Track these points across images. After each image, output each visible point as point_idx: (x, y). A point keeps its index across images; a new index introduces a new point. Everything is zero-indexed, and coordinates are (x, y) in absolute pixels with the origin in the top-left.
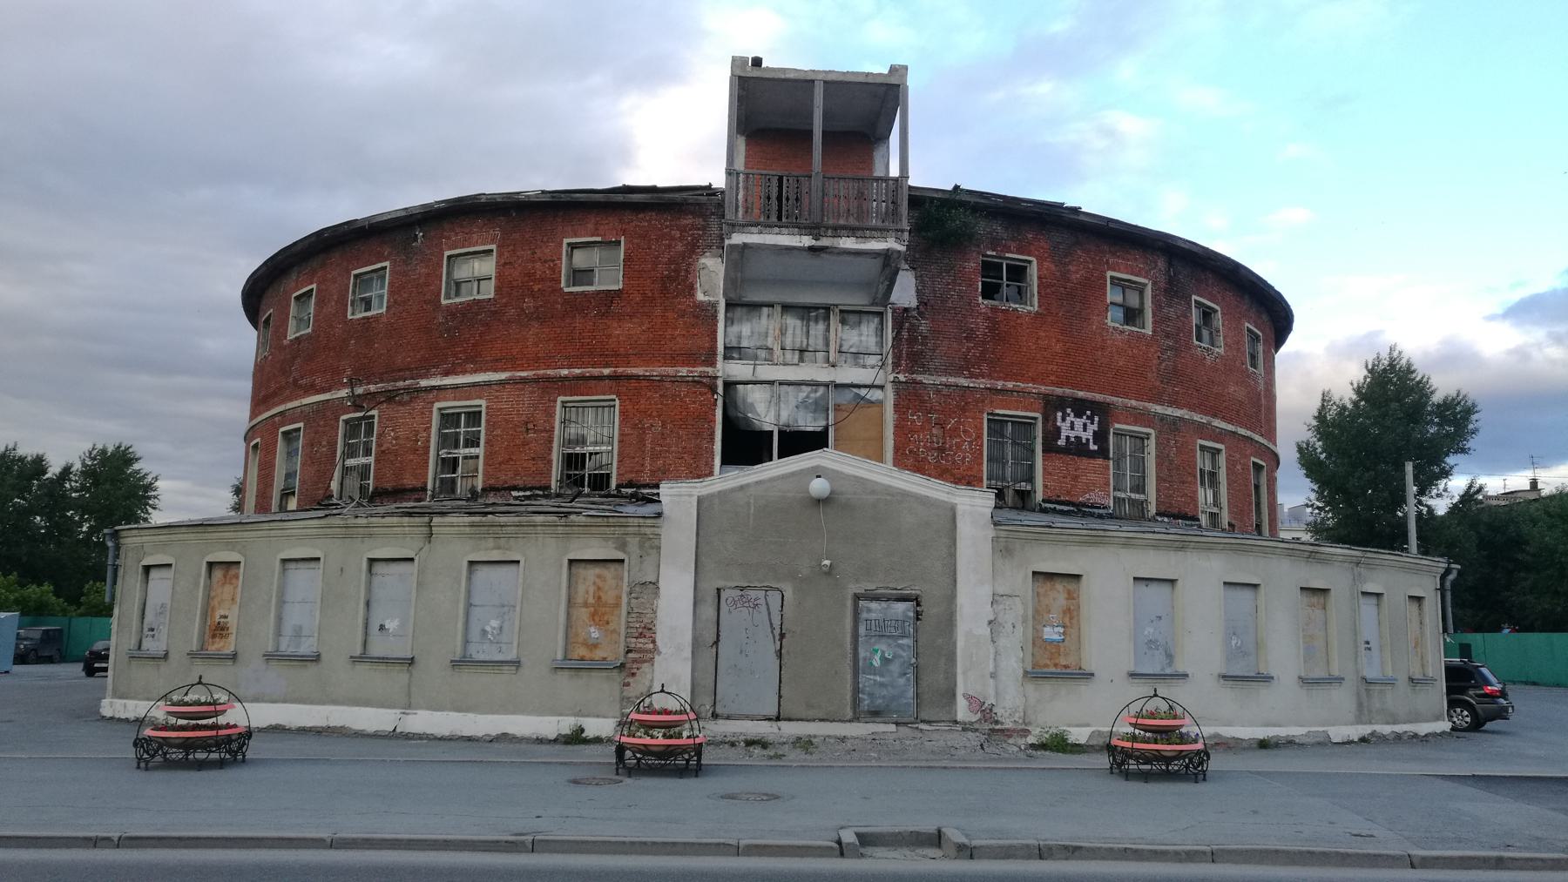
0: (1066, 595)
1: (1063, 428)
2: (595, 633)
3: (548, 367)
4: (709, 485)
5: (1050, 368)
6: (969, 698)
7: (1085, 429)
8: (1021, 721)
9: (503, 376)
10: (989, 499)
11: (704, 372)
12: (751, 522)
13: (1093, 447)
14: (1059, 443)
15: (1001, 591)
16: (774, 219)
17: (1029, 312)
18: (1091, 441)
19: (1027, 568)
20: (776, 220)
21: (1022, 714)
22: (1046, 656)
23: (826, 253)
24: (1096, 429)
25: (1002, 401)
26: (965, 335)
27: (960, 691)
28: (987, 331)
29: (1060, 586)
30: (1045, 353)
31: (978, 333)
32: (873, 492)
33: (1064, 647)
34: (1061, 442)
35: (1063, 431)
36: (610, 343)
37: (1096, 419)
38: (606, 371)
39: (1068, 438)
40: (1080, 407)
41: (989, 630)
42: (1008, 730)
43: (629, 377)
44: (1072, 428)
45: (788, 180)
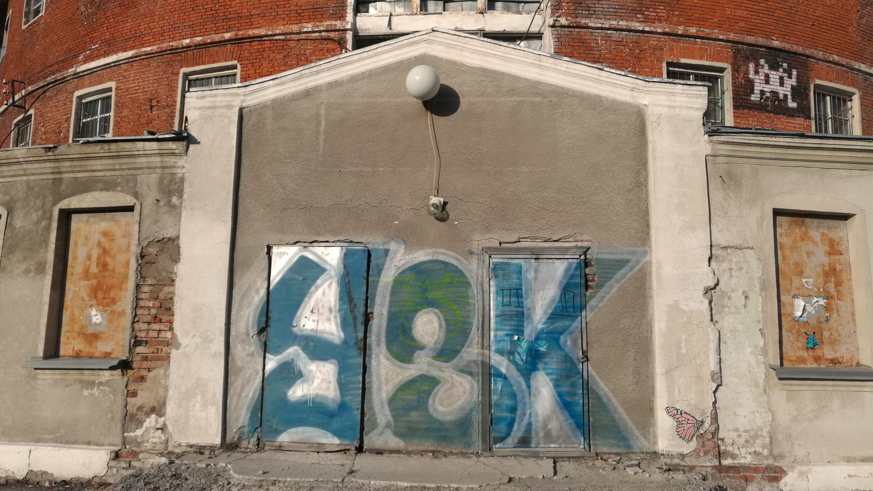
0: (827, 248)
1: (756, 81)
2: (96, 317)
3: (173, 39)
4: (258, 91)
5: (739, 13)
6: (674, 412)
7: (782, 84)
8: (766, 452)
9: (130, 54)
10: (698, 96)
11: (332, 25)
12: (322, 144)
13: (792, 104)
14: (752, 98)
15: (720, 239)
18: (789, 97)
19: (764, 204)
21: (767, 441)
22: (799, 344)
24: (795, 84)
25: (684, 48)
27: (661, 403)
29: (816, 231)
32: (512, 92)
33: (830, 329)
34: (755, 97)
35: (756, 84)
36: (233, 5)
37: (794, 72)
38: (227, 36)
39: (762, 92)
40: (775, 56)
41: (707, 302)
42: (746, 468)
43: (253, 38)
44: (767, 82)
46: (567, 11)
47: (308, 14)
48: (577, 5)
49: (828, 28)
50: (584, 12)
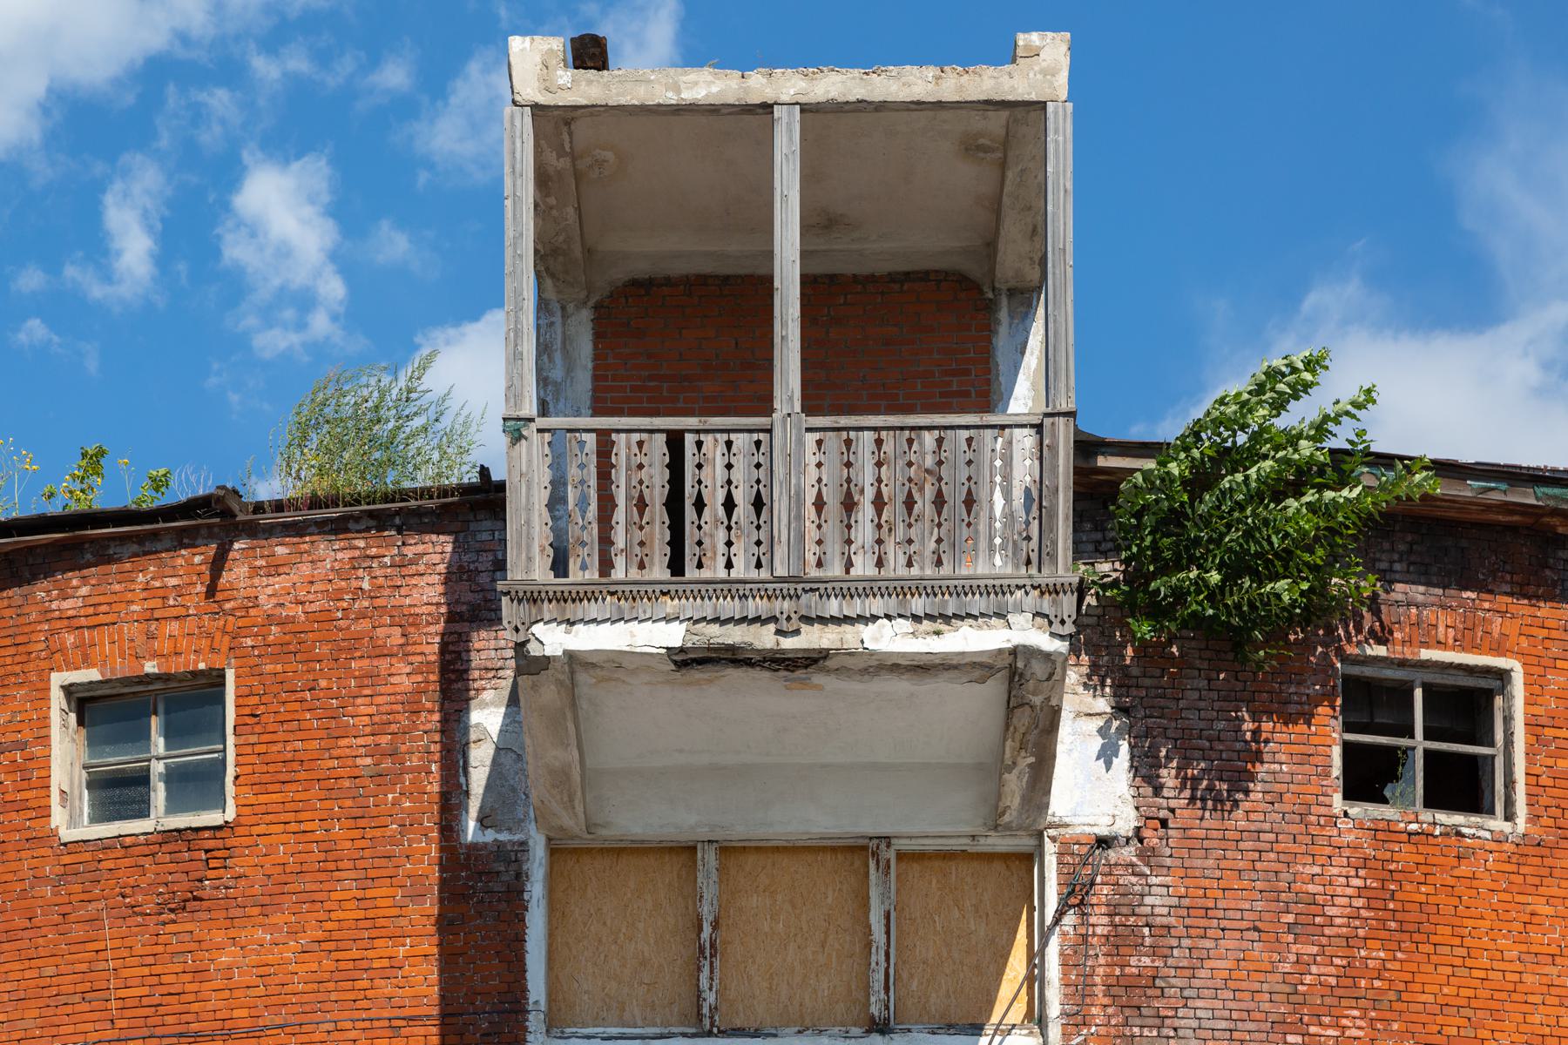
16: (659, 571)
17: (1500, 839)
20: (666, 575)
23: (828, 671)
26: (1290, 918)
28: (1359, 902)
30: (1554, 970)
31: (1330, 911)
45: (699, 444)
46: (1103, 1030)
47: (422, 1031)
48: (1127, 1012)
49: (21, 630)
50: (1146, 1032)
